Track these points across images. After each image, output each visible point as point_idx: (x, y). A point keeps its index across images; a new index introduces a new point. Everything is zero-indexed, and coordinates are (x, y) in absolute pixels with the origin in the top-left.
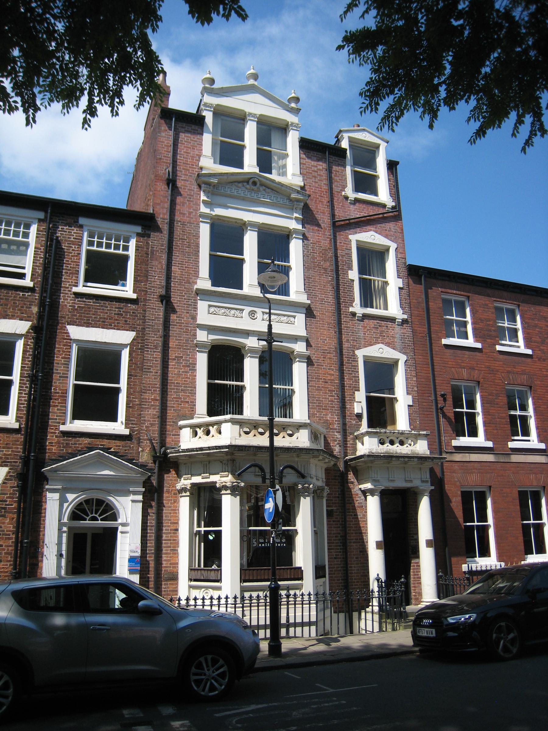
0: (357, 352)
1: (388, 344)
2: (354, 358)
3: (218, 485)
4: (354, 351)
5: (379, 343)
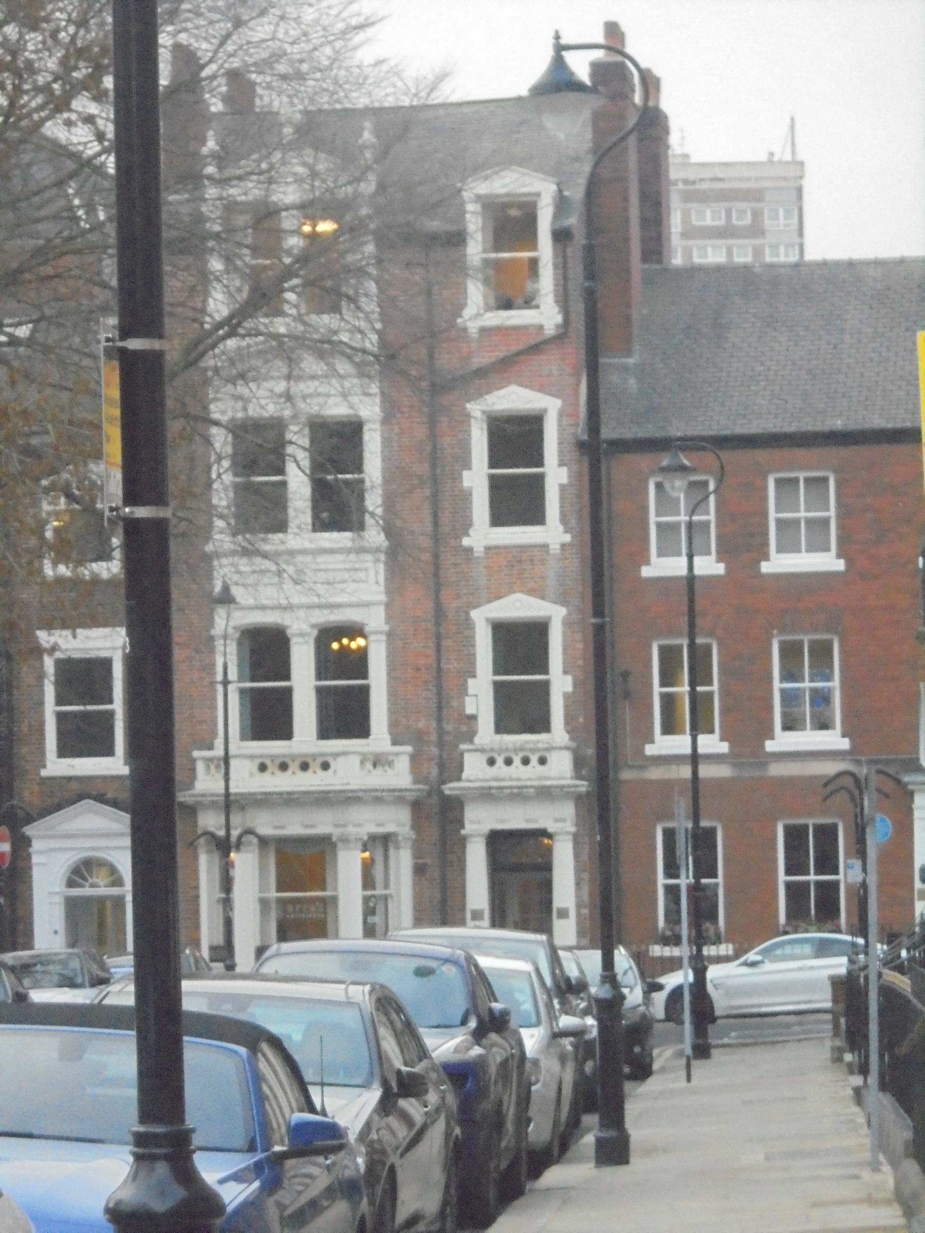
0: (475, 614)
1: (532, 592)
2: (469, 625)
3: (334, 839)
4: (467, 614)
5: (514, 592)
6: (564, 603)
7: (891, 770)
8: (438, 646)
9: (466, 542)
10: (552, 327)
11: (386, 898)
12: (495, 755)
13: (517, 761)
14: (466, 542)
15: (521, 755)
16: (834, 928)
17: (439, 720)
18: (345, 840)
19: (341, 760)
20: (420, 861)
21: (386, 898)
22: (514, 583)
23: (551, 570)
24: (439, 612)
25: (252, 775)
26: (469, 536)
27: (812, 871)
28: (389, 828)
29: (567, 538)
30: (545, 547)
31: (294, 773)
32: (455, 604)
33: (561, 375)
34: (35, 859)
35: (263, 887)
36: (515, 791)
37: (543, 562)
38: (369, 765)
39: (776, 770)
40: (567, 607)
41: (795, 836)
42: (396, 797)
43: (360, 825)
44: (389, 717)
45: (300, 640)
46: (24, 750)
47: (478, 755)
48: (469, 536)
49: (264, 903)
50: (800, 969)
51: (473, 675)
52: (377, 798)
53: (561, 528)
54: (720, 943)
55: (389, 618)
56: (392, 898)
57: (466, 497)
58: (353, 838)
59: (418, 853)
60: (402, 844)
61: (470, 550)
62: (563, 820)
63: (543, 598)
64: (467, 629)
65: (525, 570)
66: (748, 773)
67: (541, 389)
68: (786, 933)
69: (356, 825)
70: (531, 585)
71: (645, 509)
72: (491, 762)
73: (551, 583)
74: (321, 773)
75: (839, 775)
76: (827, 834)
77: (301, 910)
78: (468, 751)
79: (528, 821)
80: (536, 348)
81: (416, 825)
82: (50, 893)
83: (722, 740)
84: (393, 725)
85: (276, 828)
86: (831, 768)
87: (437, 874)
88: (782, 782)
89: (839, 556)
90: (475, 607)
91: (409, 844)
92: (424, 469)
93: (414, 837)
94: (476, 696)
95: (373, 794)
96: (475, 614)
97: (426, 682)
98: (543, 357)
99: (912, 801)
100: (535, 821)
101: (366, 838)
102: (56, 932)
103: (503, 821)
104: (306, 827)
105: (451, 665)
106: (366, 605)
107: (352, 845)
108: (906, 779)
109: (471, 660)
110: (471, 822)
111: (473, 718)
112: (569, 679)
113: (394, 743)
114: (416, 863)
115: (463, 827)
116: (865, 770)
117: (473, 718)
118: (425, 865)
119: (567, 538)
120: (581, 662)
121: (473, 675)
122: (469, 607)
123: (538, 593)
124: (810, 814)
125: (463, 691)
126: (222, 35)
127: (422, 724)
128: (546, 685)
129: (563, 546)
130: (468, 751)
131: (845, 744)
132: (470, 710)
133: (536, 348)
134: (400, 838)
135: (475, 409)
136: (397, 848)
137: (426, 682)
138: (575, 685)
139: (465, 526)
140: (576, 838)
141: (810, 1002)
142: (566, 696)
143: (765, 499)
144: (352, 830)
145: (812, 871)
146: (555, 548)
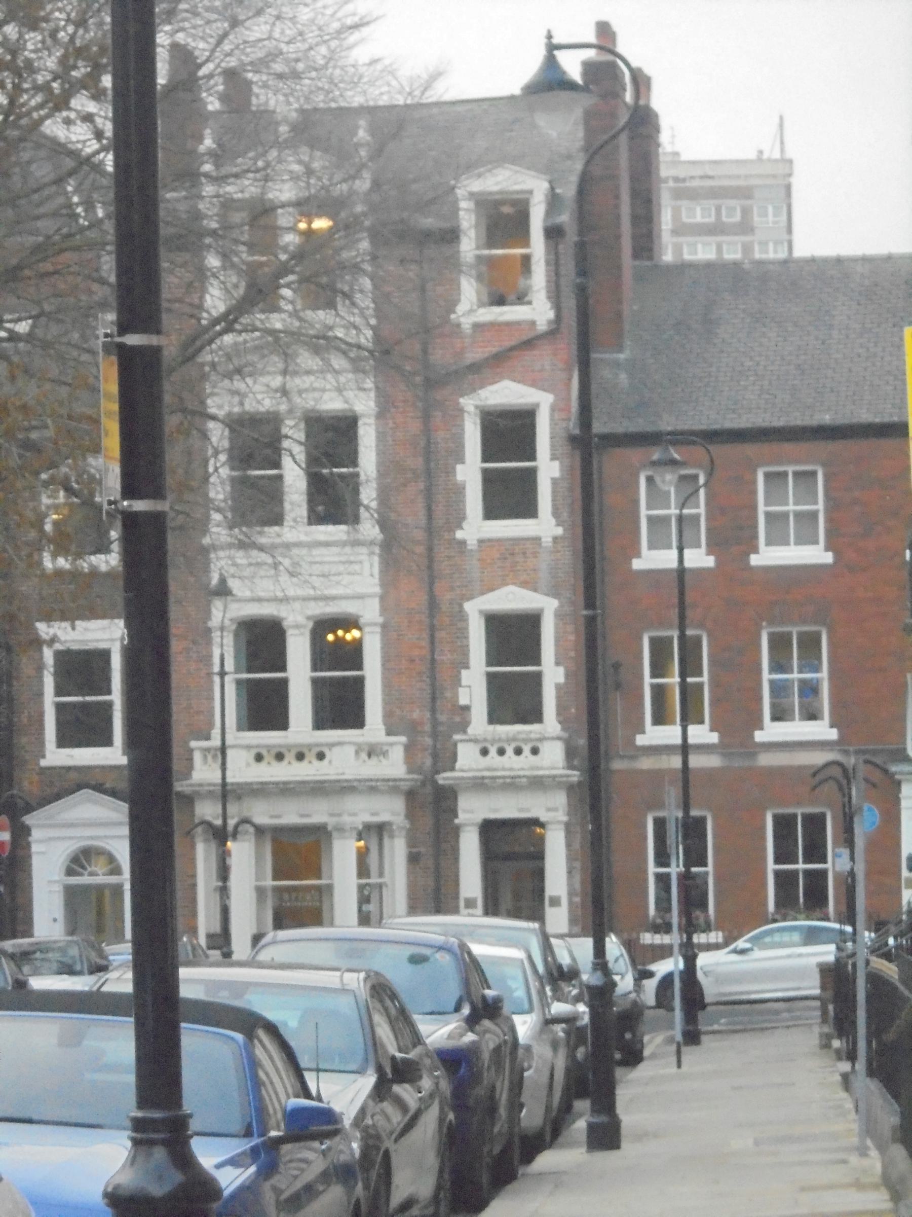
0: (468, 606)
1: (524, 584)
2: (462, 617)
3: (330, 828)
4: (461, 606)
5: (507, 584)
6: (556, 595)
7: (878, 760)
8: (432, 638)
9: (459, 535)
10: (545, 322)
11: (380, 886)
12: (488, 746)
13: (510, 751)
14: (459, 535)
15: (514, 745)
16: (822, 916)
17: (433, 711)
18: (340, 829)
19: (336, 750)
20: (414, 850)
21: (380, 886)
22: (507, 576)
23: (544, 563)
24: (433, 604)
25: (248, 765)
26: (462, 529)
27: (801, 859)
28: (384, 817)
29: (559, 531)
30: (537, 540)
31: (290, 763)
32: (448, 596)
33: (553, 370)
34: (35, 848)
35: (259, 876)
36: (508, 780)
37: (535, 554)
38: (364, 756)
39: (765, 760)
40: (559, 599)
41: (784, 825)
42: (391, 786)
43: (355, 814)
44: (384, 708)
45: (296, 632)
46: (24, 740)
47: (471, 745)
48: (462, 529)
49: (260, 891)
50: (789, 956)
51: (467, 667)
52: (371, 787)
53: (553, 521)
54: (710, 931)
55: (384, 610)
56: (387, 886)
57: (459, 491)
58: (348, 827)
59: (412, 842)
60: (397, 833)
61: (463, 543)
62: (555, 810)
63: (535, 590)
64: (460, 620)
65: (517, 562)
66: (737, 763)
67: (534, 384)
68: (775, 921)
69: (351, 815)
70: (524, 577)
71: (636, 502)
72: (485, 752)
73: (544, 576)
74: (316, 763)
75: (828, 765)
76: (815, 824)
77: (297, 898)
78: (461, 741)
79: (521, 810)
80: (529, 344)
81: (410, 814)
82: (50, 882)
83: (712, 730)
84: (388, 716)
85: (272, 817)
86: (819, 758)
87: (430, 863)
88: (771, 772)
89: (827, 549)
90: (468, 599)
91: (404, 833)
92: (418, 463)
93: (408, 826)
94: (469, 687)
95: (368, 784)
96: (468, 606)
97: (420, 674)
98: (536, 352)
99: (899, 790)
100: (528, 810)
101: (360, 827)
102: (55, 920)
103: (496, 810)
104: (302, 816)
105: (445, 657)
106: (361, 597)
107: (347, 834)
108: (893, 768)
109: (464, 651)
110: (465, 811)
111: (467, 708)
112: (561, 670)
113: (389, 733)
114: (410, 852)
115: (456, 816)
116: (852, 760)
117: (467, 708)
118: (419, 854)
119: (559, 531)
120: (572, 654)
121: (467, 667)
122: (462, 599)
123: (531, 585)
124: (799, 804)
125: (456, 682)
126: (218, 35)
127: (416, 715)
128: (538, 677)
129: (555, 539)
130: (461, 741)
131: (833, 734)
132: (463, 701)
133: (529, 344)
134: (394, 827)
135: (469, 403)
136: (392, 837)
137: (420, 674)
138: (567, 676)
139: (459, 519)
140: (568, 827)
141: (799, 989)
142: (558, 687)
143: (754, 492)
144: (347, 819)
145: (801, 859)
146: (547, 541)
